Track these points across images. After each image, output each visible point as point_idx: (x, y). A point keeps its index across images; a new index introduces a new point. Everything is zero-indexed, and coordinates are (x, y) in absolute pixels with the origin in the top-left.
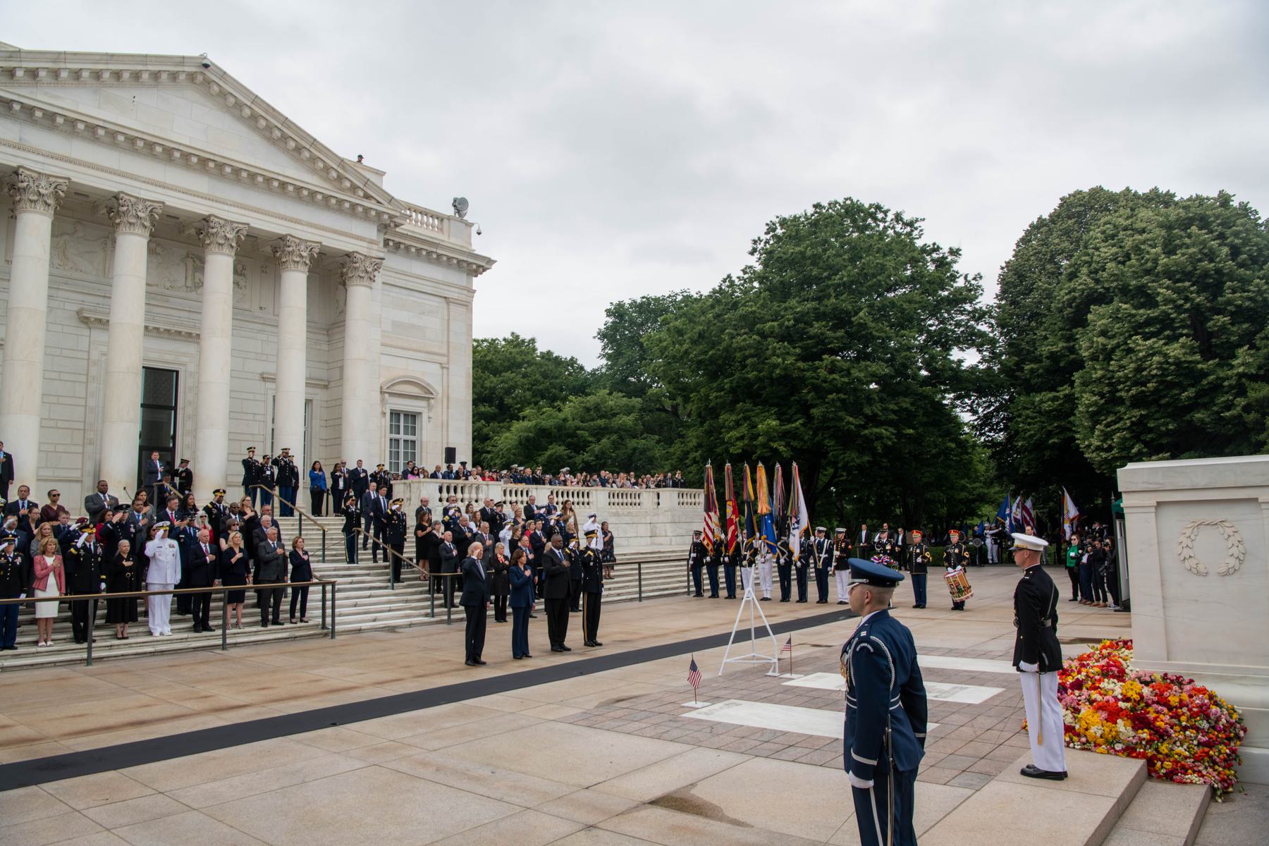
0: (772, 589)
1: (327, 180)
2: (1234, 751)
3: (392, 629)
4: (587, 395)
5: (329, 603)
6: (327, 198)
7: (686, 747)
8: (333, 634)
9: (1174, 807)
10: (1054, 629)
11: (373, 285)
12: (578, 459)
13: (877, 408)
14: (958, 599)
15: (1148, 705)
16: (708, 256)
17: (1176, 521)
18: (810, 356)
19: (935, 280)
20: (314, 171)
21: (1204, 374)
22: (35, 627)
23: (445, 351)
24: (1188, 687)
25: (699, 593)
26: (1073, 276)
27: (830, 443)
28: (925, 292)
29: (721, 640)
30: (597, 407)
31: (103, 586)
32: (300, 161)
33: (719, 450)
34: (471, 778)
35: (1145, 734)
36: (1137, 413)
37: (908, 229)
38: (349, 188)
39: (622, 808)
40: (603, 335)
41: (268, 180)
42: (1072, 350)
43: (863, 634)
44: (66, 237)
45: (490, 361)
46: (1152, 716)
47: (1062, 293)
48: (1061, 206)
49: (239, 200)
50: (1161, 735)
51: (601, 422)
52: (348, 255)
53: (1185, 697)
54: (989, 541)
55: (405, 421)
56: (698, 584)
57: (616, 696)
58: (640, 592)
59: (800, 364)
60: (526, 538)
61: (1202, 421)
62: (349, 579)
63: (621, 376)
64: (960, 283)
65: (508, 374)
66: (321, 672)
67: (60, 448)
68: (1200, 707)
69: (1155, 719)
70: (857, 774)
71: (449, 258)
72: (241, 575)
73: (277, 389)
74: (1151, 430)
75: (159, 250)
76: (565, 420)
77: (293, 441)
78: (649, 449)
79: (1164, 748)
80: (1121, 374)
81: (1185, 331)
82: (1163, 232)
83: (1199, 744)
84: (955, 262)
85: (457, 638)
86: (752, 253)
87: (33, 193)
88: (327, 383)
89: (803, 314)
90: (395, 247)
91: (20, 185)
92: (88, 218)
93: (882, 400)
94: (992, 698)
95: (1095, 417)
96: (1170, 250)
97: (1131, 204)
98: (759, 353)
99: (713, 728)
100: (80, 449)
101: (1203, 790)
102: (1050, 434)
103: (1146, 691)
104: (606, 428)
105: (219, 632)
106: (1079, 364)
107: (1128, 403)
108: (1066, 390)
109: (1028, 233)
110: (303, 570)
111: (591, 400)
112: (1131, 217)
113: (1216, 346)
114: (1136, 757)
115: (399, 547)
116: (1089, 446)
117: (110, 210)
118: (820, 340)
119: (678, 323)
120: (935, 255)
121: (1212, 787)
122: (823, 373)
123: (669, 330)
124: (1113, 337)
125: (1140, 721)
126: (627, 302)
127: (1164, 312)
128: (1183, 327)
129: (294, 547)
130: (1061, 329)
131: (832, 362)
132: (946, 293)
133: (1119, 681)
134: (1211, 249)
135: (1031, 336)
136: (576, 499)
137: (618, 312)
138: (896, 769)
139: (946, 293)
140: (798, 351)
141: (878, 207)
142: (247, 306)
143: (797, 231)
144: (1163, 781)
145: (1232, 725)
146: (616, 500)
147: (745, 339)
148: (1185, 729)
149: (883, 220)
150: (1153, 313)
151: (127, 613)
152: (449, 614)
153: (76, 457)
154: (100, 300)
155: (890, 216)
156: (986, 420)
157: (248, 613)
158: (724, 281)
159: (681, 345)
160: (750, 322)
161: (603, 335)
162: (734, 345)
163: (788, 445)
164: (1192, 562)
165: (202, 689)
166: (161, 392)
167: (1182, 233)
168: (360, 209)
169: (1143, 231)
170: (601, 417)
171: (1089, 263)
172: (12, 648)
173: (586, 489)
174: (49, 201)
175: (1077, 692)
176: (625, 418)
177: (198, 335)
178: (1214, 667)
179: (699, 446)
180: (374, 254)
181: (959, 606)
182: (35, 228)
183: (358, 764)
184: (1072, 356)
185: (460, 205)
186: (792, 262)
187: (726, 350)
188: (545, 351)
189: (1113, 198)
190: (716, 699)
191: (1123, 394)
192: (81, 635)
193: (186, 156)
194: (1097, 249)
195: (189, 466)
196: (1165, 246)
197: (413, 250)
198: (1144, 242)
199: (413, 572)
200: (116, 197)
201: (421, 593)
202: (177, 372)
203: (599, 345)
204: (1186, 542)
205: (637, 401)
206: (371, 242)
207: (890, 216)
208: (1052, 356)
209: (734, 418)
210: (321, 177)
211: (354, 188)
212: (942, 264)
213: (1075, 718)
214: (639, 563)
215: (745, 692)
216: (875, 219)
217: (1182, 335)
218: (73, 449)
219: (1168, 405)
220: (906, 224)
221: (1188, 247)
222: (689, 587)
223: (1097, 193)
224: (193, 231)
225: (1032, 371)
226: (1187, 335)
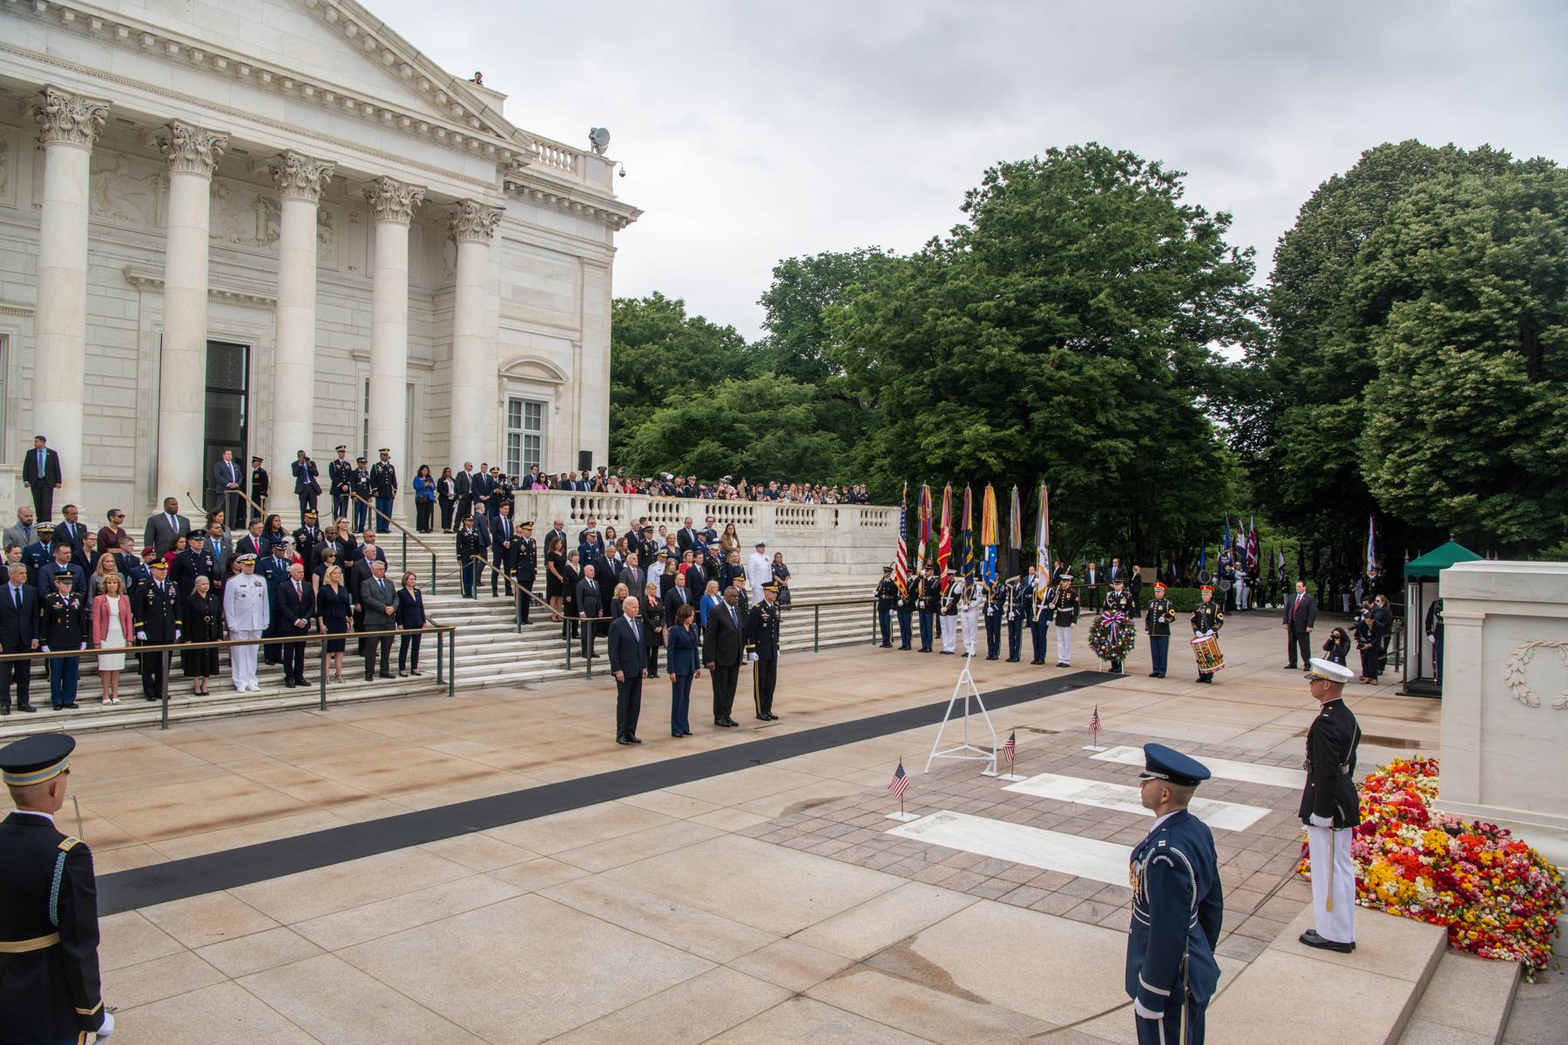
0: (975, 641)
1: (433, 104)
2: (1552, 922)
3: (520, 685)
4: (746, 378)
5: (446, 650)
6: (433, 129)
7: (898, 881)
8: (452, 690)
9: (1481, 988)
10: (1351, 773)
11: (491, 241)
12: (737, 458)
13: (1113, 416)
14: (1205, 670)
15: (1454, 861)
16: (909, 201)
17: (1508, 641)
18: (1033, 346)
19: (1196, 255)
20: (417, 94)
21: (1530, 399)
22: (97, 679)
23: (577, 325)
24: (1503, 842)
25: (887, 643)
26: (1371, 258)
27: (1052, 456)
28: (1185, 270)
29: (930, 715)
30: (760, 395)
31: (178, 634)
32: (400, 80)
33: (913, 458)
34: (647, 917)
35: (1448, 897)
36: (1441, 442)
37: (1165, 185)
38: (463, 116)
39: (832, 969)
40: (769, 301)
41: (360, 105)
42: (1362, 353)
43: (1162, 843)
44: (108, 174)
45: (627, 329)
46: (1458, 875)
47: (1357, 278)
48: (1362, 163)
49: (324, 131)
50: (1468, 899)
51: (764, 414)
52: (459, 203)
53: (1500, 854)
54: (1238, 585)
55: (526, 412)
56: (886, 631)
57: (804, 797)
58: (817, 639)
59: (1021, 356)
60: (681, 576)
61: (1521, 457)
62: (467, 619)
63: (795, 365)
64: (1227, 258)
65: (649, 346)
66: (445, 748)
67: (107, 441)
68: (1518, 868)
69: (1462, 879)
70: (1145, 1004)
71: (585, 207)
72: (342, 618)
73: (371, 371)
74: (1456, 465)
75: (223, 192)
76: (720, 409)
77: (392, 439)
78: (824, 450)
79: (1470, 916)
80: (1425, 392)
81: (1511, 343)
82: (1495, 213)
83: (1513, 912)
84: (1223, 231)
85: (606, 696)
86: (965, 209)
87: (66, 120)
88: (433, 363)
89: (1028, 293)
90: (519, 190)
91: (49, 109)
92: (136, 152)
93: (1118, 406)
94: (1257, 824)
95: (1386, 444)
96: (1501, 237)
97: (1453, 166)
98: (969, 339)
99: (928, 853)
100: (131, 443)
101: (1514, 969)
102: (1326, 457)
103: (1453, 843)
104: (771, 421)
105: (317, 686)
106: (1373, 372)
107: (1430, 429)
108: (1350, 404)
109: (1317, 196)
110: (410, 611)
111: (753, 384)
112: (1453, 185)
113: (1549, 363)
114: (1436, 923)
115: (527, 579)
116: (1376, 479)
117: (162, 142)
118: (1046, 326)
119: (868, 296)
120: (1196, 221)
121: (1523, 964)
122: (1048, 368)
123: (856, 304)
124: (1419, 343)
125: (1443, 881)
126: (801, 259)
127: (1487, 316)
128: (1509, 337)
129: (404, 584)
130: (1351, 325)
131: (1061, 356)
132: (1209, 271)
133: (1420, 827)
134: (1554, 239)
135: (1311, 330)
136: (736, 516)
137: (788, 272)
138: (1192, 1000)
139: (1209, 271)
140: (1019, 339)
141: (1131, 158)
142: (332, 265)
143: (1025, 185)
144: (1465, 955)
145: (1552, 890)
146: (785, 518)
147: (954, 322)
148: (1498, 893)
149: (1136, 173)
150: (1473, 317)
151: (204, 665)
152: (589, 665)
153: (133, 468)
154: (152, 256)
155: (1145, 167)
156: (1244, 433)
157: (349, 662)
158: (929, 244)
159: (872, 324)
160: (960, 300)
161: (769, 301)
162: (939, 329)
163: (999, 456)
164: (1522, 690)
165: (309, 769)
166: (228, 371)
167: (1519, 215)
168: (475, 144)
169: (1467, 205)
170: (765, 407)
171: (1395, 243)
172: (72, 706)
173: (749, 504)
174: (88, 131)
175: (1368, 839)
176: (795, 410)
177: (274, 303)
178: (1535, 818)
179: (889, 452)
180: (493, 202)
181: (1205, 678)
182: (69, 166)
183: (512, 892)
184: (1362, 361)
185: (599, 138)
186: (1016, 226)
187: (929, 333)
188: (695, 316)
189: (1431, 157)
190: (924, 809)
191: (1425, 417)
192: (154, 690)
193: (257, 73)
194: (1406, 225)
195: (263, 466)
196: (1495, 229)
197: (540, 195)
198: (1468, 224)
199: (542, 611)
200: (169, 125)
201: (554, 637)
202: (248, 348)
203: (763, 312)
204: (1517, 664)
205: (810, 388)
206: (489, 186)
207: (1145, 167)
208: (1338, 360)
209: (933, 419)
210: (427, 101)
211: (468, 116)
212: (1205, 233)
213: (1365, 870)
214: (817, 606)
215: (959, 800)
216: (1126, 173)
217: (1506, 348)
218: (122, 442)
219: (1481, 434)
220: (1163, 179)
221: (1524, 234)
222: (874, 633)
223: (1410, 147)
224: (265, 169)
225: (1310, 376)
226: (1513, 348)
